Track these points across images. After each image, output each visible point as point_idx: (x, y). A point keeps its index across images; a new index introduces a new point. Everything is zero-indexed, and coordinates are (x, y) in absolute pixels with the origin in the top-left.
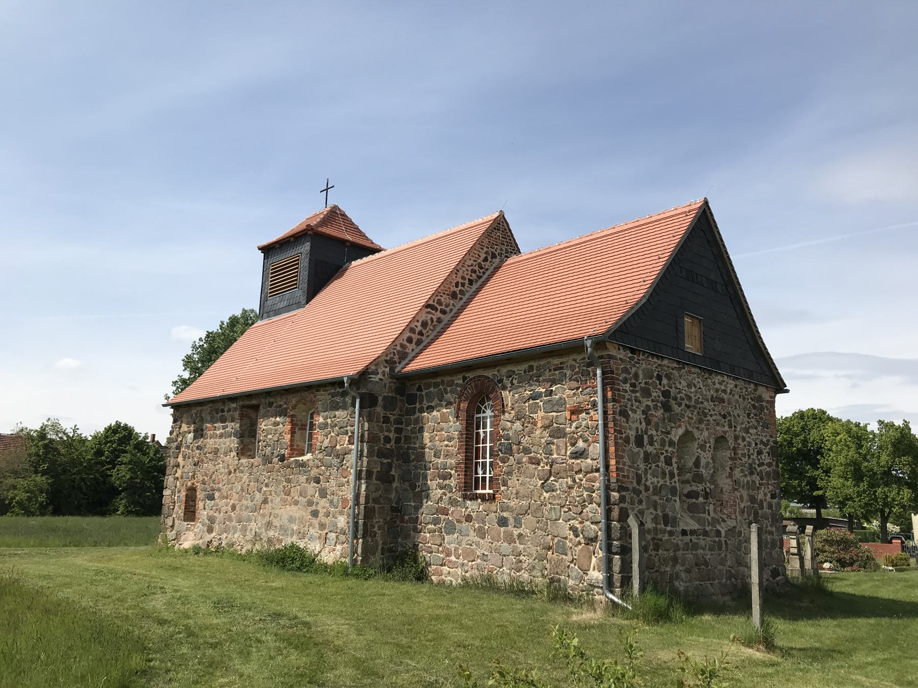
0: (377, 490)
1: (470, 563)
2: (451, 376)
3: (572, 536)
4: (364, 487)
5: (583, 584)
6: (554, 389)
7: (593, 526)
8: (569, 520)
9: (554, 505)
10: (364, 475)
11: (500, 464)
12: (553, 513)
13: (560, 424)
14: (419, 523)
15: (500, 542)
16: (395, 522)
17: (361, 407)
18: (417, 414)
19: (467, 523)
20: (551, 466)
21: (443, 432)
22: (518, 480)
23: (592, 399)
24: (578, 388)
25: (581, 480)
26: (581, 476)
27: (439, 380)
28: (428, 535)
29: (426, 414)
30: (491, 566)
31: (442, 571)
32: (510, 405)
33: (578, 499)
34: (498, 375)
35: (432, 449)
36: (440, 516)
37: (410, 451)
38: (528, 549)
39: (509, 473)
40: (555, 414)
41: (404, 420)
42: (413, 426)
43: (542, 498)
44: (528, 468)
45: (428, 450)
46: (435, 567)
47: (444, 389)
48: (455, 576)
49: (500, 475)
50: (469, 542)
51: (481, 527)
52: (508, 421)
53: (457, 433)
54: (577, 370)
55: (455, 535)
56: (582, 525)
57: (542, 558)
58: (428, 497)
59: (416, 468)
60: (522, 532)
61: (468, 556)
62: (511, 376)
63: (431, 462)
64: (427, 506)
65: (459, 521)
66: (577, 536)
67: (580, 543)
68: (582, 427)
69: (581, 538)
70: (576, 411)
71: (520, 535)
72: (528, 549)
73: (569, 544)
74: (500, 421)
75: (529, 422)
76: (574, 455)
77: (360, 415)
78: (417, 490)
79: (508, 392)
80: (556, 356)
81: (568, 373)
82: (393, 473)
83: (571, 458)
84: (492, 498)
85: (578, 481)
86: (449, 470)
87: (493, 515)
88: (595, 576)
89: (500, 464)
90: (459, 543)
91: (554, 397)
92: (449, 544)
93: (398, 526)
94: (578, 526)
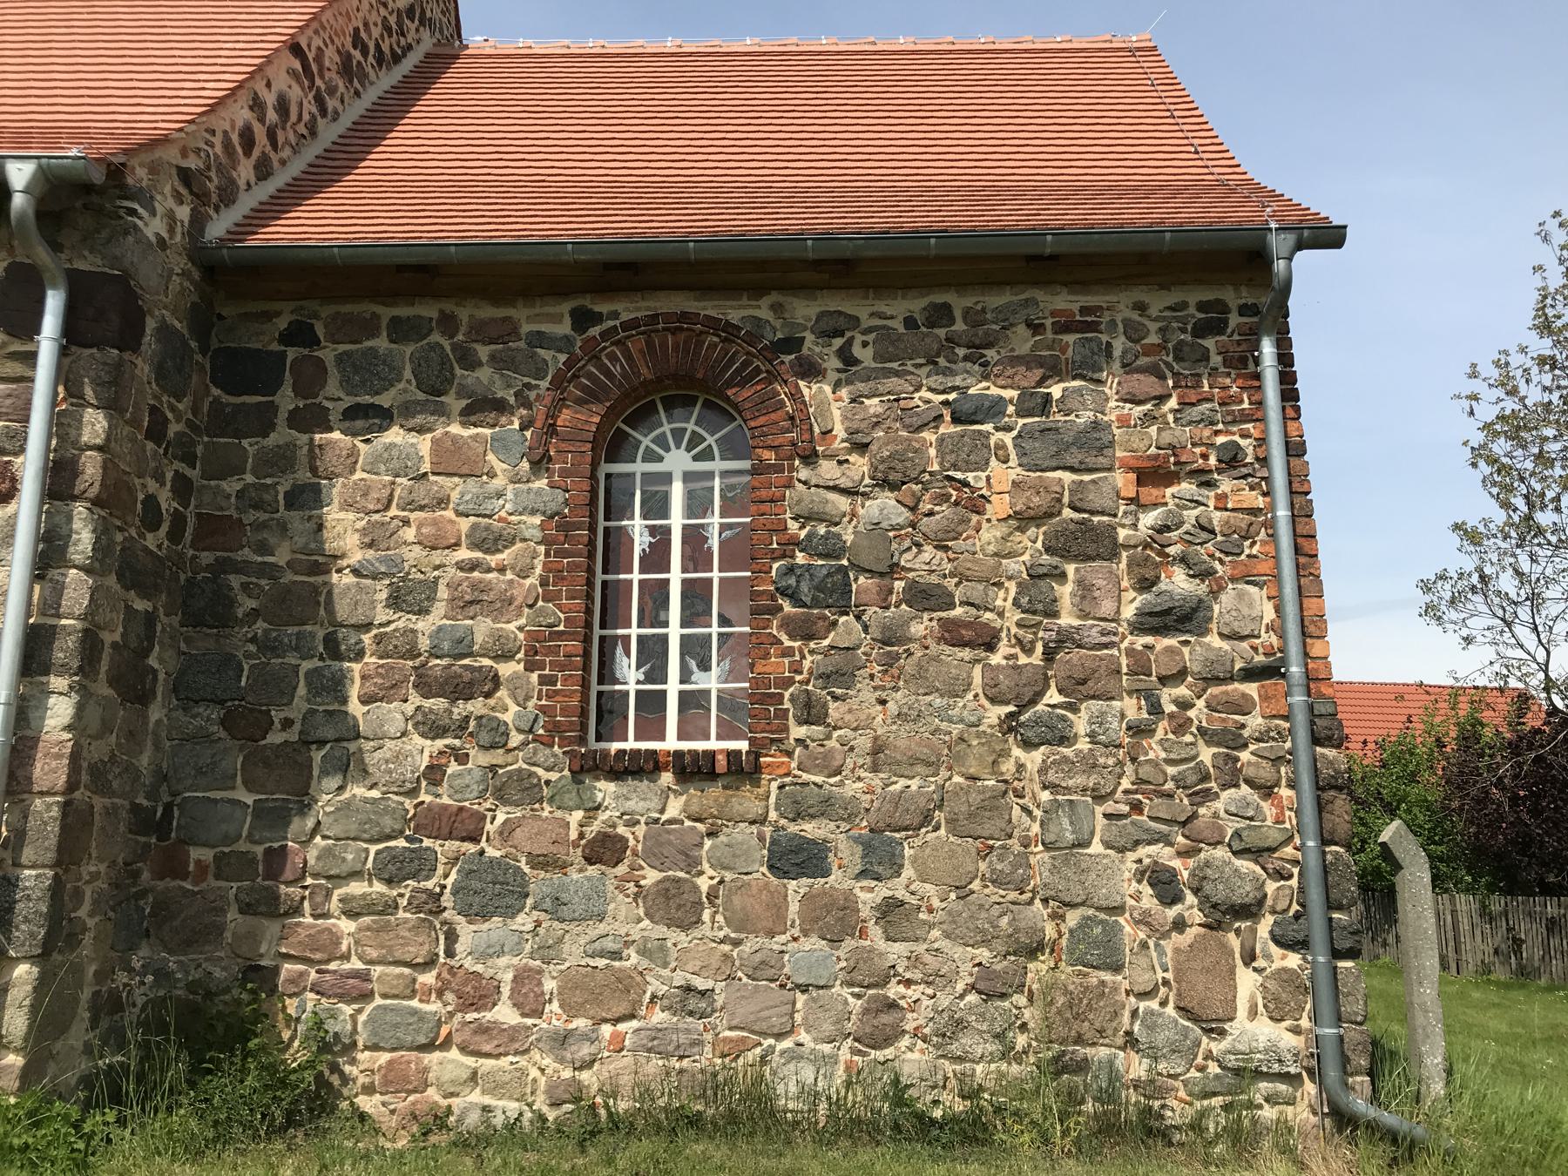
0: (106, 728)
1: (606, 1030)
2: (497, 301)
3: (1149, 901)
4: (59, 711)
5: (1202, 1069)
6: (1056, 391)
7: (1245, 865)
8: (1137, 843)
9: (1068, 790)
10: (65, 649)
11: (788, 643)
12: (1066, 822)
13: (1092, 513)
14: (288, 874)
15: (783, 938)
16: (136, 875)
17: (71, 334)
18: (281, 434)
19: (592, 871)
20: (1049, 655)
21: (449, 514)
22: (883, 702)
23: (1220, 440)
24: (1162, 399)
25: (1184, 705)
26: (1182, 691)
27: (428, 311)
28: (347, 926)
29: (336, 435)
30: (728, 1033)
31: (426, 1070)
32: (839, 431)
33: (1171, 770)
34: (778, 324)
35: (375, 577)
36: (427, 842)
37: (235, 581)
38: (928, 958)
39: (839, 676)
40: (1068, 477)
41: (199, 450)
42: (249, 478)
43: (1008, 767)
44: (936, 659)
45: (348, 579)
46: (384, 1057)
47: (454, 347)
48: (516, 1086)
49: (791, 682)
50: (609, 944)
51: (678, 881)
52: (835, 489)
53: (537, 520)
54: (1153, 339)
55: (524, 921)
56: (1191, 862)
57: (991, 988)
58: (348, 766)
59: (268, 646)
60: (901, 894)
61: (596, 998)
62: (839, 333)
63: (367, 626)
64: (347, 804)
65: (542, 862)
66: (1176, 899)
67: (1180, 925)
68: (1186, 527)
69: (1190, 906)
70: (1153, 474)
71: (890, 910)
72: (928, 958)
73: (1130, 933)
74: (789, 486)
75: (945, 498)
76: (1155, 621)
77: (65, 375)
78: (275, 738)
79: (828, 389)
80: (1065, 284)
81: (1119, 345)
82: (152, 661)
83: (1138, 627)
84: (743, 771)
85: (1170, 708)
86: (486, 662)
87: (743, 833)
88: (1262, 1039)
89: (788, 643)
90: (548, 952)
91: (1058, 417)
92: (483, 956)
93: (143, 894)
94: (1176, 863)
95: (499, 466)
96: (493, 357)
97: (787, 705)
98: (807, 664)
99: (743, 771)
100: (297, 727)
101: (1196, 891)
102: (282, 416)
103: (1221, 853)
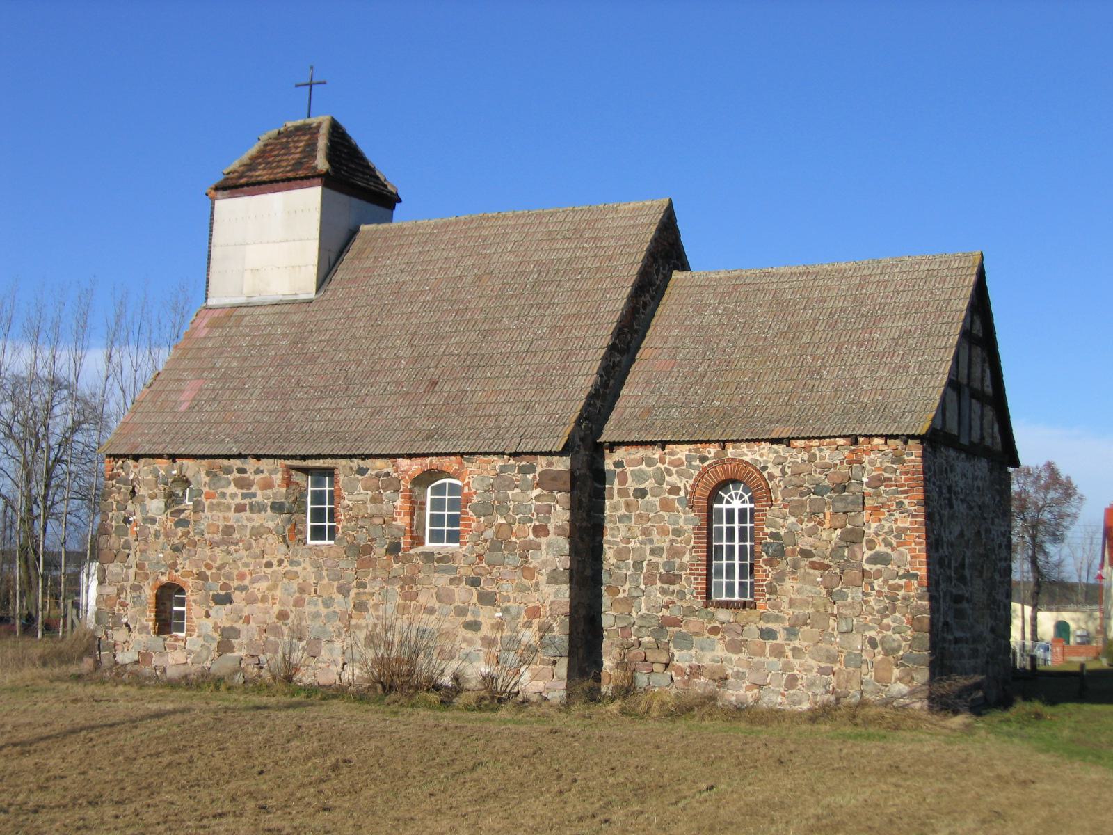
39: (780, 578)
55: (693, 652)
78: (621, 595)
95: (680, 509)
96: (677, 472)
97: (764, 588)
98: (770, 575)
99: (753, 605)
100: (627, 592)
101: (882, 644)
102: (616, 491)
103: (890, 633)
